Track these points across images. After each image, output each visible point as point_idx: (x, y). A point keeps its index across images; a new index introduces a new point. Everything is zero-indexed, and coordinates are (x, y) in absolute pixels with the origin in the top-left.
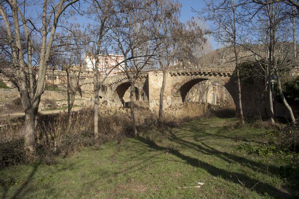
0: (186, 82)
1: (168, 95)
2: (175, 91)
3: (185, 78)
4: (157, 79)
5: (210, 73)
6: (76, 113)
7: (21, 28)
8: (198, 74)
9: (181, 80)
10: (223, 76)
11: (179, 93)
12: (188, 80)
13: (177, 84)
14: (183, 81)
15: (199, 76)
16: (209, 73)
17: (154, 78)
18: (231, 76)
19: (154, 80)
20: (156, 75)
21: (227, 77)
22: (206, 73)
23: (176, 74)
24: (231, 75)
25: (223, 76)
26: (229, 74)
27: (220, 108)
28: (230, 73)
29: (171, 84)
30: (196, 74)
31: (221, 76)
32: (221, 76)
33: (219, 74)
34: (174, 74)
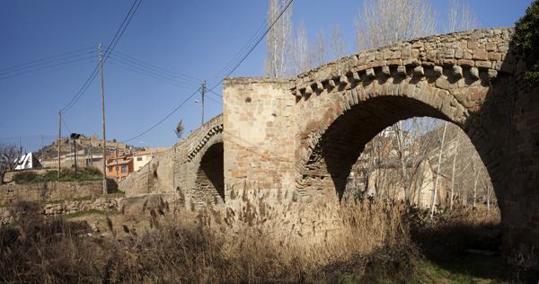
0: (336, 116)
1: (285, 169)
2: (306, 154)
3: (333, 102)
4: (250, 114)
5: (414, 65)
6: (98, 197)
7: (460, 86)
8: (371, 78)
9: (324, 108)
10: (462, 82)
11: (321, 164)
12: (344, 106)
13: (312, 127)
14: (326, 116)
15: (391, 88)
16: (410, 67)
17: (241, 110)
18: (494, 81)
19: (243, 119)
20: (249, 100)
21: (479, 89)
22: (402, 69)
23: (309, 89)
24: (493, 73)
25: (462, 82)
26: (483, 70)
27: (442, 219)
28: (488, 64)
29: (296, 130)
30: (365, 78)
31: (454, 78)
32: (454, 78)
33: (448, 68)
34: (303, 91)
